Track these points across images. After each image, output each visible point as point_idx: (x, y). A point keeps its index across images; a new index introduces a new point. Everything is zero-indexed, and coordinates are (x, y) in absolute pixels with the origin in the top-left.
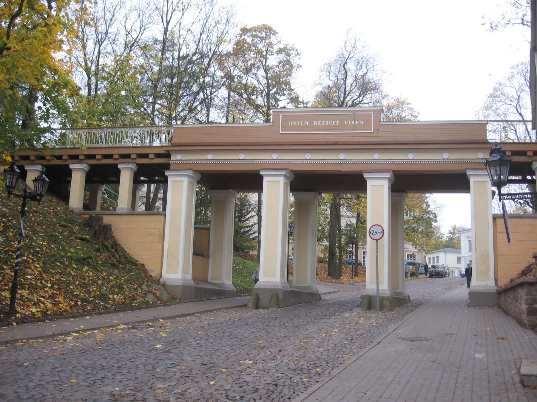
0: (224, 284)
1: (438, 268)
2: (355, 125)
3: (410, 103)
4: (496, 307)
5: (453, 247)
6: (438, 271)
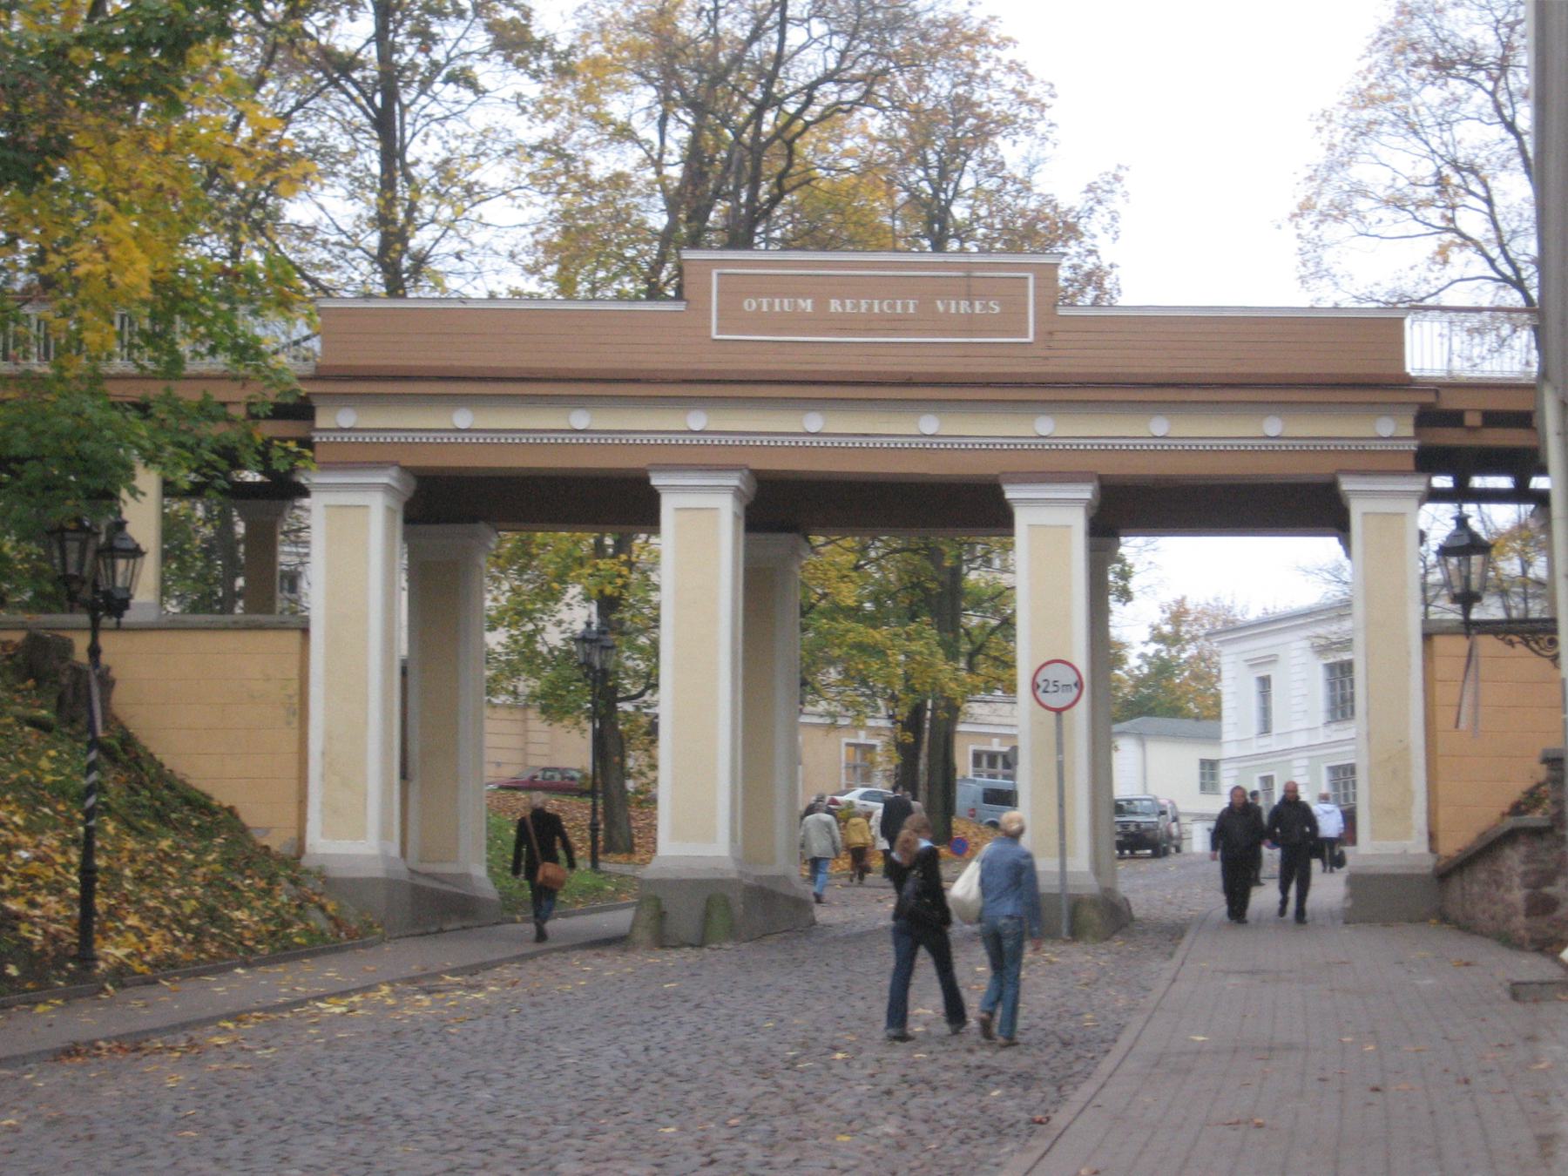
0: (468, 876)
1: (1135, 813)
2: (970, 317)
3: (1015, 37)
4: (1434, 921)
5: (1175, 711)
6: (1138, 825)
